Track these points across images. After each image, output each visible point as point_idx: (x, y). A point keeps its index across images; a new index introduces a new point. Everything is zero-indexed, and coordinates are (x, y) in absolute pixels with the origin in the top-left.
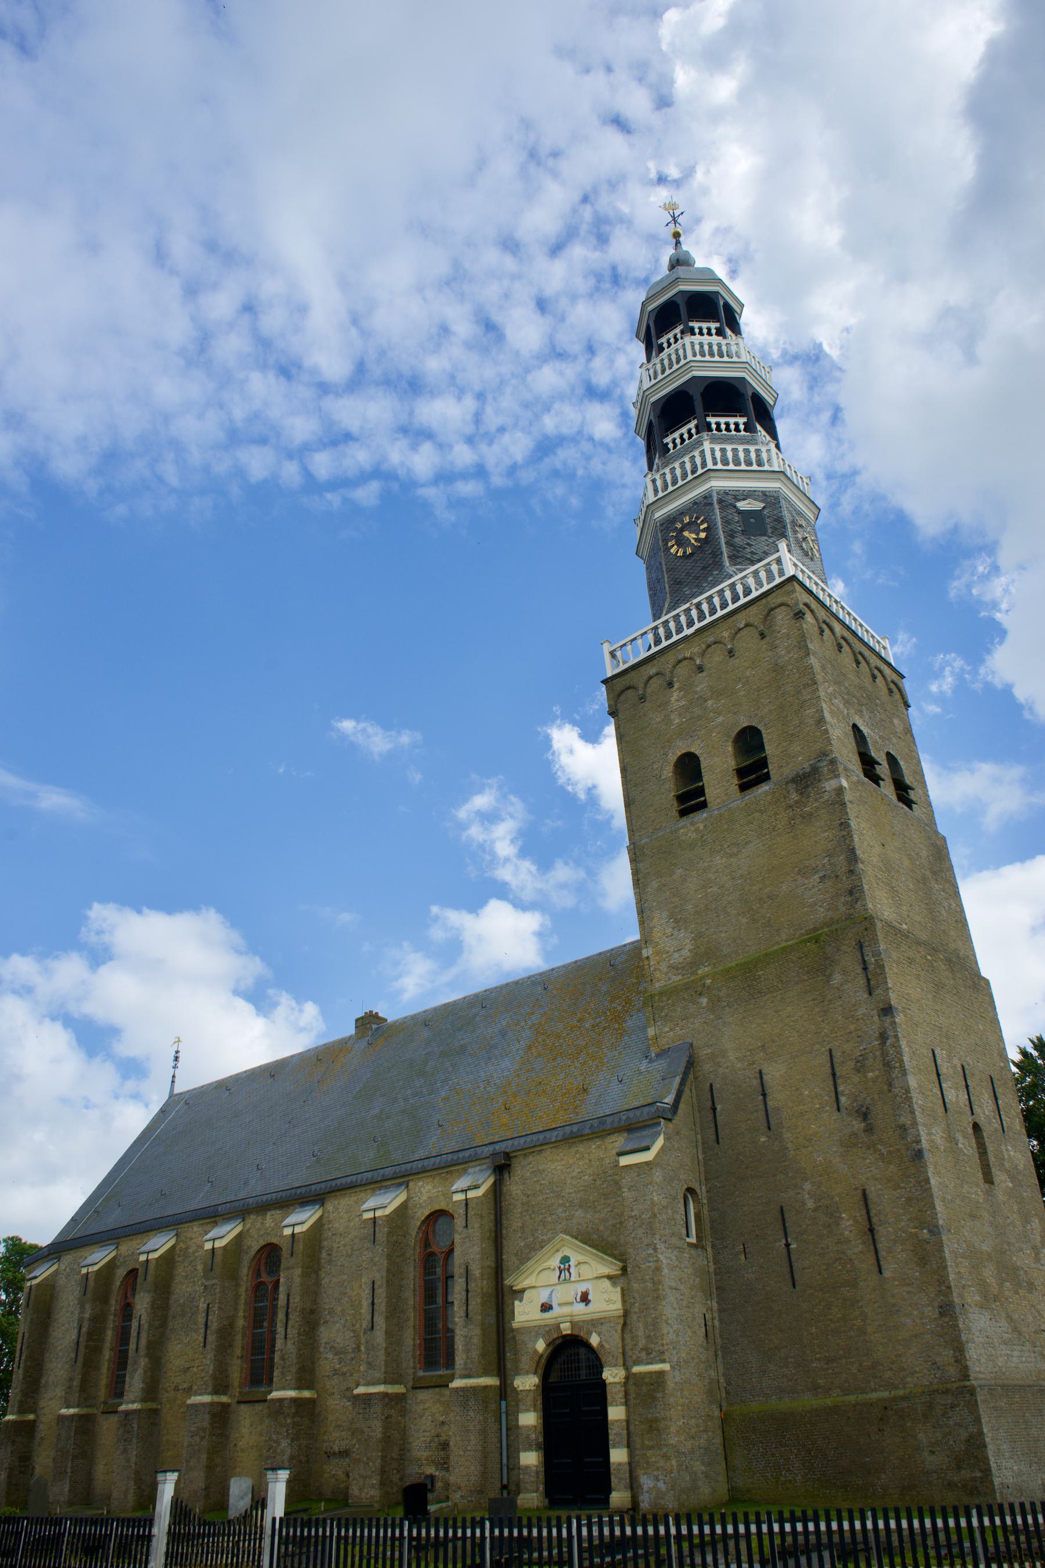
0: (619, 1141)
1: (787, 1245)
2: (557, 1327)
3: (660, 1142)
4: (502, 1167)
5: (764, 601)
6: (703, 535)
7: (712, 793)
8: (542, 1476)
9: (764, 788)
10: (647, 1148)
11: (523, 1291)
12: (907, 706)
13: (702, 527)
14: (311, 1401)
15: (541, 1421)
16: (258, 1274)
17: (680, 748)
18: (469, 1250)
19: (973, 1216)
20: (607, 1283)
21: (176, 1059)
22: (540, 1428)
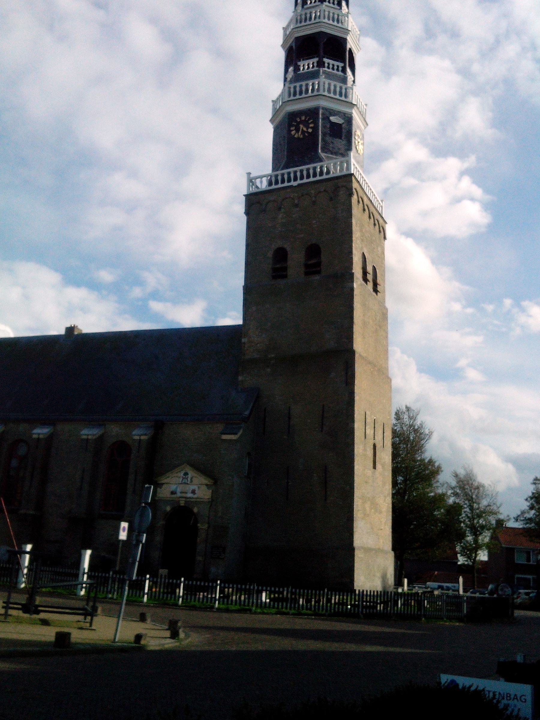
0: (220, 427)
1: (288, 483)
3: (241, 431)
4: (159, 427)
5: (336, 181)
6: (310, 130)
7: (291, 272)
9: (317, 277)
10: (236, 434)
12: (385, 238)
17: (279, 243)
19: (366, 482)
20: (205, 488)
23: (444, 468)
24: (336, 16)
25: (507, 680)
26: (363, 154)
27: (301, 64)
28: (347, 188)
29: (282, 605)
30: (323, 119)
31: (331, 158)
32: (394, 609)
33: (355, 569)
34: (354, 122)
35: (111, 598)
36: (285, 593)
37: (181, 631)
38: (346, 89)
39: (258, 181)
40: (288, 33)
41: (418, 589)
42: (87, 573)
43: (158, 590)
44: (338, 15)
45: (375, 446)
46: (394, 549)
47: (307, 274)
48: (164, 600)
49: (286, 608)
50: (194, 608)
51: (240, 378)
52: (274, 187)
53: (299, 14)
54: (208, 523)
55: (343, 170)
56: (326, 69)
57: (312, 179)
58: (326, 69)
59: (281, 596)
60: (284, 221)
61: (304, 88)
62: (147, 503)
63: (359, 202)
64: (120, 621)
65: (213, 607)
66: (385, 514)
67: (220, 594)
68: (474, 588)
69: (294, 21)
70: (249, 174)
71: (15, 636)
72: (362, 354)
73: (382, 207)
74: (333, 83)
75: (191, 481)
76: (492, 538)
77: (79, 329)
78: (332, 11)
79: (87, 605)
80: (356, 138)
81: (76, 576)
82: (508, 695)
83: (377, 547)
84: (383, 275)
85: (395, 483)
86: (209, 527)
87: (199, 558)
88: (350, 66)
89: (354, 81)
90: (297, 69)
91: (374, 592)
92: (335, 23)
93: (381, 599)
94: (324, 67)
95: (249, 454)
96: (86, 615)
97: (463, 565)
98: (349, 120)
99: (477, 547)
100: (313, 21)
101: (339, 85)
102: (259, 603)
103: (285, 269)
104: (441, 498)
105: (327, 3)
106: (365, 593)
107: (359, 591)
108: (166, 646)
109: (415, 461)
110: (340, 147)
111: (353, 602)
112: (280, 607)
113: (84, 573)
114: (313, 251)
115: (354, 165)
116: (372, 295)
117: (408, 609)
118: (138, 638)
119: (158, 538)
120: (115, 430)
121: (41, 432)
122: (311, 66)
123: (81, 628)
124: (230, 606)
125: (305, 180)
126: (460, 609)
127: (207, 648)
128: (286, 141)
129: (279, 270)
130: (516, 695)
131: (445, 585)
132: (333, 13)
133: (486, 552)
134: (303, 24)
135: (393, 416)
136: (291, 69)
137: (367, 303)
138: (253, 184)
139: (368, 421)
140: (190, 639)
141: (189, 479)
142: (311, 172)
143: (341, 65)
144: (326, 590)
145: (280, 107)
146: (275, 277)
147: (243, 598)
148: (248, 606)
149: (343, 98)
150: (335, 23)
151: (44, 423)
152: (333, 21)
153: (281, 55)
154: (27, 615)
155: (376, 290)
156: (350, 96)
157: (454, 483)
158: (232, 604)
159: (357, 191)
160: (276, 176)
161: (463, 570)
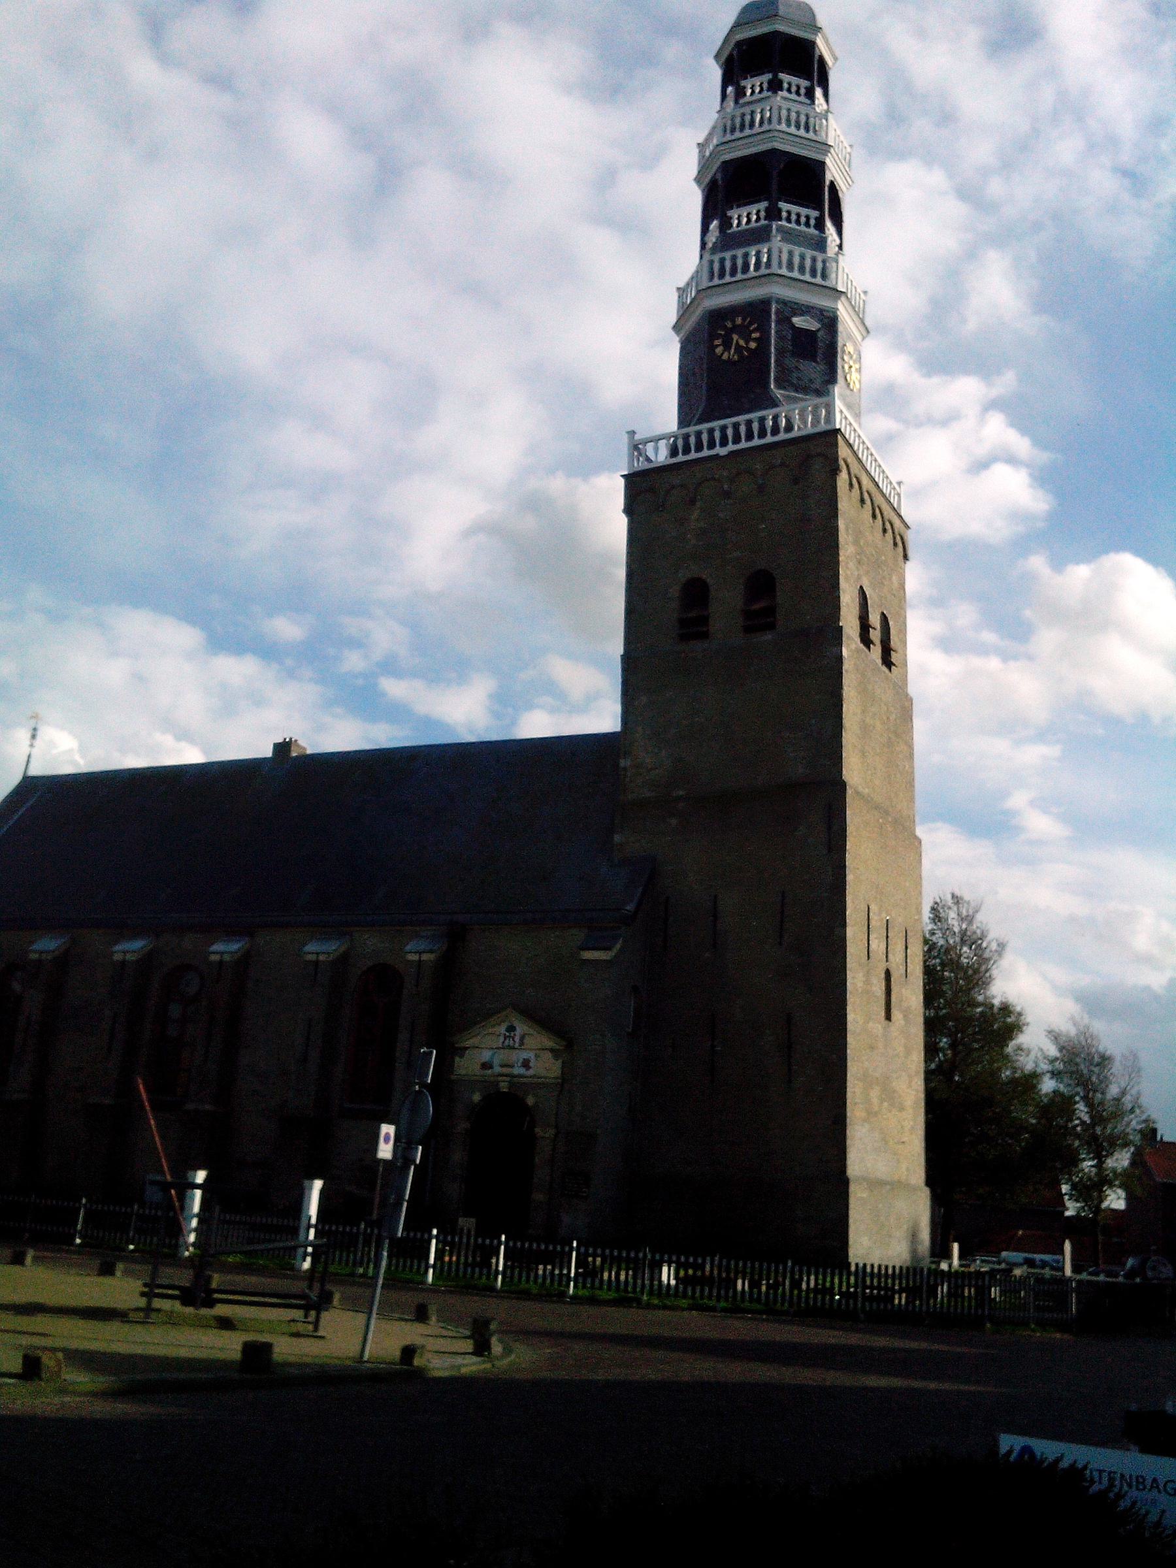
1: (713, 1046)
4: (456, 936)
6: (753, 345)
7: (717, 625)
9: (768, 636)
10: (608, 949)
11: (466, 1048)
12: (906, 557)
13: (754, 335)
19: (872, 1048)
20: (549, 1055)
23: (1029, 1018)
24: (803, 119)
25: (1143, 1450)
26: (860, 390)
27: (734, 214)
28: (826, 457)
29: (702, 1291)
30: (778, 322)
31: (795, 400)
32: (928, 1304)
33: (851, 1221)
34: (840, 328)
35: (362, 1276)
36: (708, 1268)
37: (494, 1340)
38: (824, 262)
39: (650, 448)
40: (707, 154)
41: (980, 1265)
42: (316, 1226)
43: (454, 1258)
44: (807, 116)
45: (888, 974)
46: (930, 1182)
47: (748, 630)
48: (466, 1280)
49: (710, 1297)
50: (525, 1295)
51: (617, 838)
52: (681, 458)
53: (729, 116)
54: (556, 1127)
55: (819, 422)
56: (784, 223)
57: (756, 442)
58: (784, 223)
59: (699, 1273)
60: (702, 524)
61: (740, 262)
62: (423, 1085)
63: (851, 485)
64: (373, 1322)
65: (563, 1294)
66: (911, 1111)
67: (577, 1268)
68: (1097, 1265)
69: (719, 131)
71: (161, 1351)
72: (860, 789)
73: (899, 495)
74: (797, 251)
75: (522, 1043)
76: (1133, 1163)
77: (298, 746)
78: (795, 107)
79: (310, 1287)
80: (846, 358)
81: (294, 1231)
82: (1140, 1480)
83: (896, 1178)
84: (903, 631)
85: (931, 1050)
86: (556, 1135)
87: (539, 1197)
88: (832, 216)
89: (840, 247)
90: (725, 223)
91: (887, 1267)
92: (802, 132)
93: (900, 1284)
94: (780, 220)
95: (635, 989)
96: (307, 1308)
97: (1077, 1217)
98: (830, 322)
99: (1102, 1181)
100: (757, 129)
101: (809, 253)
102: (656, 1287)
103: (704, 620)
104: (1030, 1081)
105: (785, 93)
106: (869, 1270)
107: (857, 1265)
108: (464, 1370)
109: (974, 1004)
110: (813, 376)
111: (844, 1289)
112: (698, 1294)
113: (309, 1226)
114: (761, 585)
115: (841, 412)
116: (879, 670)
117: (956, 1302)
118: (409, 1352)
119: (458, 1156)
120: (372, 944)
121: (225, 949)
122: (754, 217)
123: (297, 1335)
124: (598, 1292)
125: (743, 445)
126: (1063, 1303)
127: (546, 1374)
128: (705, 366)
129: (693, 626)
130: (1155, 1480)
131: (1038, 1257)
132: (798, 113)
133: (1121, 1193)
134: (738, 134)
135: (926, 914)
136: (715, 224)
137: (870, 687)
138: (640, 454)
139: (873, 923)
140: (513, 1356)
141: (517, 1039)
142: (755, 426)
143: (814, 214)
144: (790, 1264)
145: (693, 301)
146: (684, 638)
147: (623, 1277)
148: (634, 1291)
149: (818, 280)
150: (802, 132)
151: (231, 931)
152: (798, 127)
153: (695, 200)
154: (190, 1310)
155: (888, 662)
156: (833, 276)
157: (1053, 1051)
158: (601, 1288)
159: (848, 466)
160: (686, 437)
161: (1073, 1228)
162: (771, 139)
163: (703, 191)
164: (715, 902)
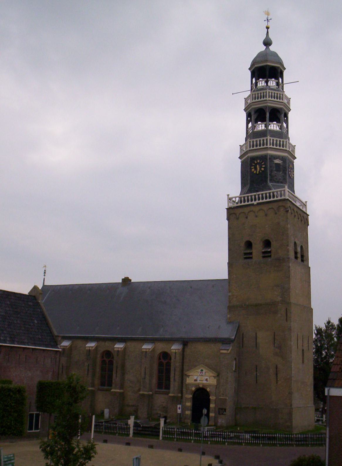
1: (257, 374)
2: (199, 385)
8: (191, 417)
9: (269, 259)
11: (189, 376)
12: (308, 225)
14: (123, 393)
15: (191, 405)
16: (103, 357)
18: (175, 363)
20: (213, 378)
21: (45, 273)
22: (191, 406)
45: (303, 350)
70: (228, 195)
110: (280, 177)
114: (248, 256)
132: (274, 93)
141: (204, 373)
152: (274, 98)
162: (267, 103)
163: (246, 114)
164: (256, 335)
